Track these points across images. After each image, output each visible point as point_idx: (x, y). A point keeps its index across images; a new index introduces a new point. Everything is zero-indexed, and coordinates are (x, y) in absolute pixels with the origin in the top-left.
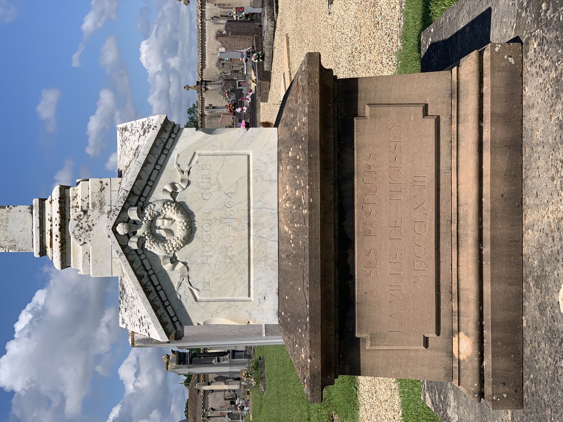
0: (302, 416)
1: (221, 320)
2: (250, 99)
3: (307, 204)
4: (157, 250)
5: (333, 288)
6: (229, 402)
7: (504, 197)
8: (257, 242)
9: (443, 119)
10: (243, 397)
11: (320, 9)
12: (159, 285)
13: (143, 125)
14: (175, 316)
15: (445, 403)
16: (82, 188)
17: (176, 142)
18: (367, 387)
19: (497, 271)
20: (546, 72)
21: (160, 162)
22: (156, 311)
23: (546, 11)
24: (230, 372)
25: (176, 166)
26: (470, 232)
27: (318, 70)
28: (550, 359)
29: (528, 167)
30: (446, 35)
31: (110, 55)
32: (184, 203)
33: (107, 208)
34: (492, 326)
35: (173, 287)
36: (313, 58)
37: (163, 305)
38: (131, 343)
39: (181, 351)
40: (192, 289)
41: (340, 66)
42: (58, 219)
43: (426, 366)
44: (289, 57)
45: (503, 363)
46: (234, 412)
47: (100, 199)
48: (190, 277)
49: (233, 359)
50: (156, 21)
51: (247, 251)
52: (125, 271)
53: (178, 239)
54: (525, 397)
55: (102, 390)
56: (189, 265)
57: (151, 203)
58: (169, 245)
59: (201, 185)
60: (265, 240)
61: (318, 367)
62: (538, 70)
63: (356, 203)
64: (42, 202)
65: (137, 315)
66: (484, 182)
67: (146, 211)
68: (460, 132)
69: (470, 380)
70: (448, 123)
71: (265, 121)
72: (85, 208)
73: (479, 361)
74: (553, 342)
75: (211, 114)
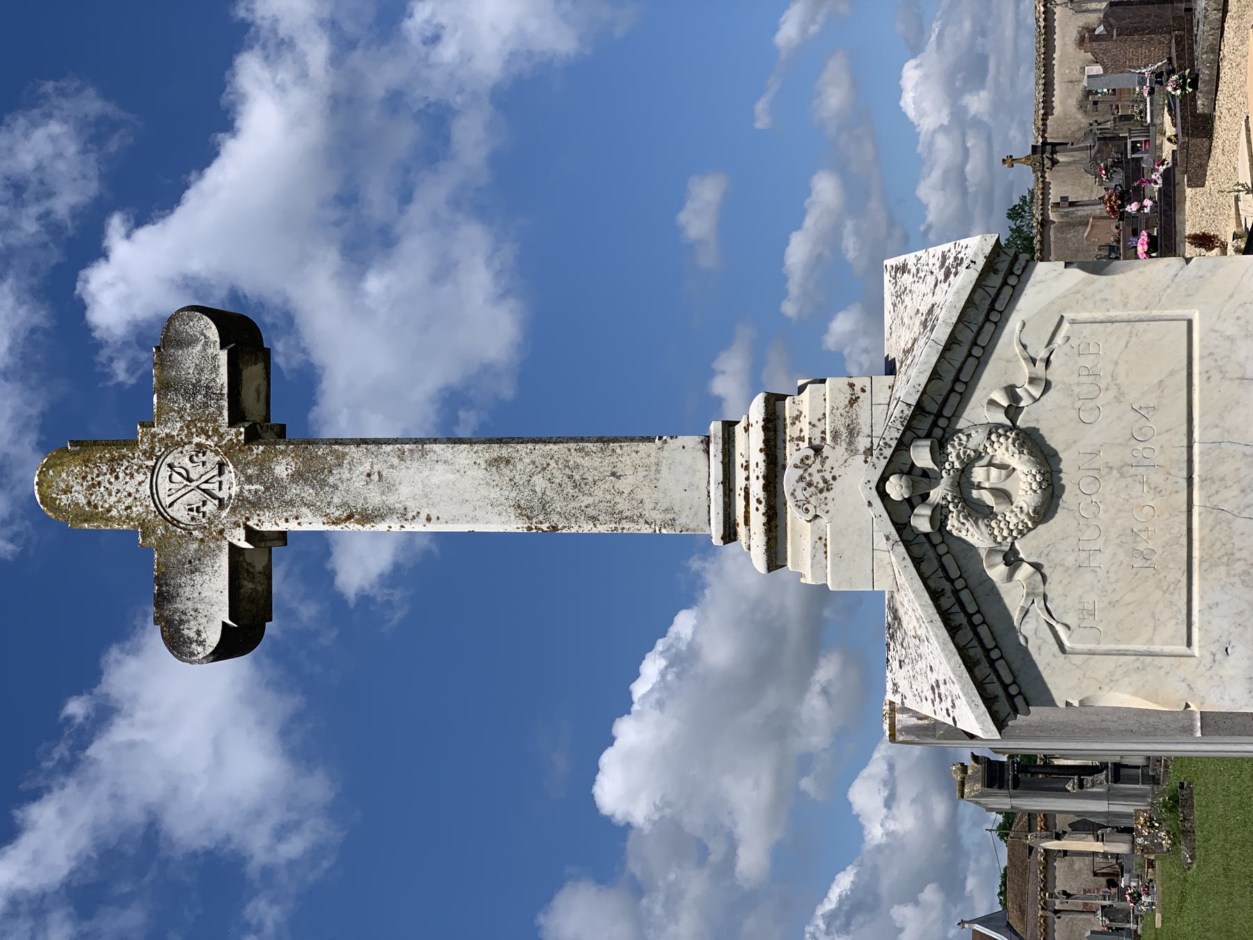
2: (1160, 181)
4: (974, 535)
6: (1103, 880)
8: (1210, 521)
10: (1139, 872)
12: (979, 612)
13: (944, 258)
14: (1014, 682)
16: (812, 398)
17: (1020, 295)
21: (982, 341)
24: (1108, 814)
25: (1018, 349)
31: (834, 97)
32: (1036, 430)
33: (862, 443)
35: (1010, 618)
37: (988, 656)
38: (888, 733)
39: (994, 757)
40: (1054, 623)
42: (762, 466)
46: (1117, 904)
47: (848, 421)
48: (1049, 595)
49: (1116, 782)
50: (938, 14)
52: (902, 580)
53: (1022, 511)
55: (814, 833)
56: (1046, 571)
57: (960, 431)
58: (1002, 525)
59: (1076, 389)
60: (1229, 516)
64: (729, 427)
65: (928, 676)
67: (950, 449)
72: (817, 442)
75: (1065, 220)
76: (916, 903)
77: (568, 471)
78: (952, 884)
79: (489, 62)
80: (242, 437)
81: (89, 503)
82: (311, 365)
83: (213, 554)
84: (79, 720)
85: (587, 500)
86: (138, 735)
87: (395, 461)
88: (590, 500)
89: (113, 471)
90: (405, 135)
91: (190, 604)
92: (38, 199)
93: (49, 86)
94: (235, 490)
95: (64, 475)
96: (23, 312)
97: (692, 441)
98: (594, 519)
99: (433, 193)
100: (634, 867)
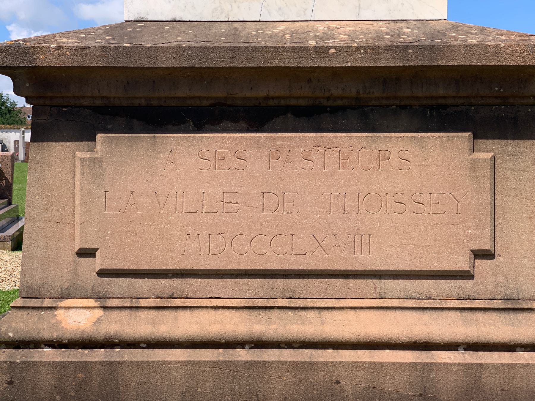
5: (180, 94)
7: (336, 385)
9: (467, 285)
19: (207, 372)
26: (274, 327)
34: (111, 362)
45: (46, 381)
63: (325, 134)
68: (445, 313)
70: (460, 293)
73: (52, 341)
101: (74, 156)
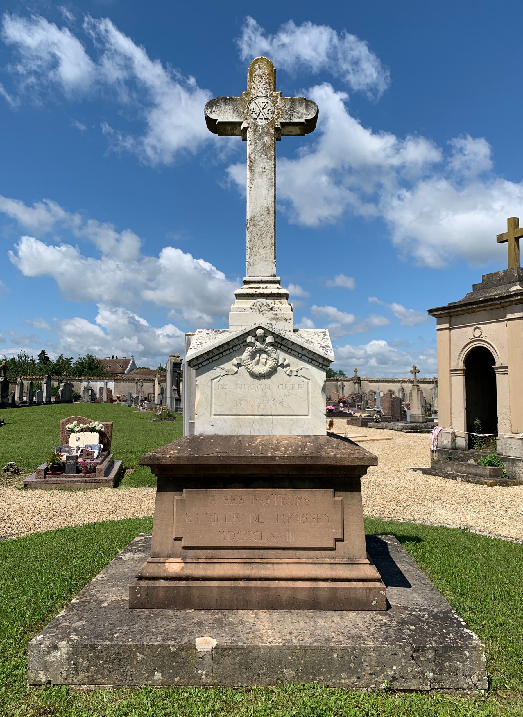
0: (134, 447)
1: (198, 396)
3: (275, 455)
4: (246, 355)
5: (217, 473)
6: (147, 396)
9: (333, 553)
11: (410, 462)
15: (136, 550)
16: (287, 307)
18: (151, 493)
19: (227, 591)
20: (366, 629)
22: (205, 353)
23: (409, 629)
24: (166, 397)
25: (300, 367)
26: (254, 572)
27: (366, 464)
28: (163, 629)
29: (299, 614)
30: (392, 554)
31: (377, 321)
33: (273, 322)
35: (221, 365)
36: (374, 461)
37: (210, 358)
39: (182, 365)
41: (372, 476)
42: (267, 292)
43: (162, 539)
44: (377, 440)
45: (162, 594)
46: (140, 400)
51: (244, 414)
52: (232, 334)
54: (137, 610)
59: (288, 384)
61: (164, 462)
62: (368, 622)
64: (278, 282)
65: (204, 341)
66: (289, 582)
67: (271, 348)
68: (324, 565)
69: (151, 570)
71: (334, 422)
72: (274, 309)
74: (175, 632)
76: (139, 343)
77: (265, 233)
78: (145, 354)
79: (391, 216)
80: (276, 126)
81: (256, 75)
82: (299, 159)
83: (239, 116)
84: (188, 82)
85: (256, 239)
86: (183, 101)
87: (269, 177)
88: (256, 239)
89: (266, 83)
90: (369, 189)
91: (223, 108)
92: (353, 70)
93: (388, 74)
94: (260, 124)
95: (265, 67)
96: (318, 64)
97: (274, 271)
98: (251, 241)
99: (352, 198)
100: (146, 259)
101: (174, 498)
